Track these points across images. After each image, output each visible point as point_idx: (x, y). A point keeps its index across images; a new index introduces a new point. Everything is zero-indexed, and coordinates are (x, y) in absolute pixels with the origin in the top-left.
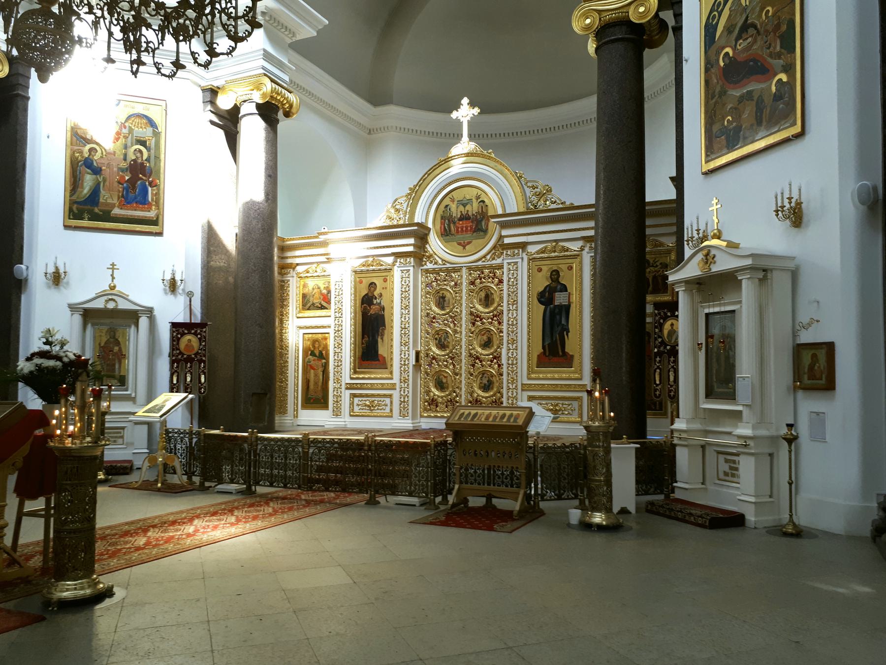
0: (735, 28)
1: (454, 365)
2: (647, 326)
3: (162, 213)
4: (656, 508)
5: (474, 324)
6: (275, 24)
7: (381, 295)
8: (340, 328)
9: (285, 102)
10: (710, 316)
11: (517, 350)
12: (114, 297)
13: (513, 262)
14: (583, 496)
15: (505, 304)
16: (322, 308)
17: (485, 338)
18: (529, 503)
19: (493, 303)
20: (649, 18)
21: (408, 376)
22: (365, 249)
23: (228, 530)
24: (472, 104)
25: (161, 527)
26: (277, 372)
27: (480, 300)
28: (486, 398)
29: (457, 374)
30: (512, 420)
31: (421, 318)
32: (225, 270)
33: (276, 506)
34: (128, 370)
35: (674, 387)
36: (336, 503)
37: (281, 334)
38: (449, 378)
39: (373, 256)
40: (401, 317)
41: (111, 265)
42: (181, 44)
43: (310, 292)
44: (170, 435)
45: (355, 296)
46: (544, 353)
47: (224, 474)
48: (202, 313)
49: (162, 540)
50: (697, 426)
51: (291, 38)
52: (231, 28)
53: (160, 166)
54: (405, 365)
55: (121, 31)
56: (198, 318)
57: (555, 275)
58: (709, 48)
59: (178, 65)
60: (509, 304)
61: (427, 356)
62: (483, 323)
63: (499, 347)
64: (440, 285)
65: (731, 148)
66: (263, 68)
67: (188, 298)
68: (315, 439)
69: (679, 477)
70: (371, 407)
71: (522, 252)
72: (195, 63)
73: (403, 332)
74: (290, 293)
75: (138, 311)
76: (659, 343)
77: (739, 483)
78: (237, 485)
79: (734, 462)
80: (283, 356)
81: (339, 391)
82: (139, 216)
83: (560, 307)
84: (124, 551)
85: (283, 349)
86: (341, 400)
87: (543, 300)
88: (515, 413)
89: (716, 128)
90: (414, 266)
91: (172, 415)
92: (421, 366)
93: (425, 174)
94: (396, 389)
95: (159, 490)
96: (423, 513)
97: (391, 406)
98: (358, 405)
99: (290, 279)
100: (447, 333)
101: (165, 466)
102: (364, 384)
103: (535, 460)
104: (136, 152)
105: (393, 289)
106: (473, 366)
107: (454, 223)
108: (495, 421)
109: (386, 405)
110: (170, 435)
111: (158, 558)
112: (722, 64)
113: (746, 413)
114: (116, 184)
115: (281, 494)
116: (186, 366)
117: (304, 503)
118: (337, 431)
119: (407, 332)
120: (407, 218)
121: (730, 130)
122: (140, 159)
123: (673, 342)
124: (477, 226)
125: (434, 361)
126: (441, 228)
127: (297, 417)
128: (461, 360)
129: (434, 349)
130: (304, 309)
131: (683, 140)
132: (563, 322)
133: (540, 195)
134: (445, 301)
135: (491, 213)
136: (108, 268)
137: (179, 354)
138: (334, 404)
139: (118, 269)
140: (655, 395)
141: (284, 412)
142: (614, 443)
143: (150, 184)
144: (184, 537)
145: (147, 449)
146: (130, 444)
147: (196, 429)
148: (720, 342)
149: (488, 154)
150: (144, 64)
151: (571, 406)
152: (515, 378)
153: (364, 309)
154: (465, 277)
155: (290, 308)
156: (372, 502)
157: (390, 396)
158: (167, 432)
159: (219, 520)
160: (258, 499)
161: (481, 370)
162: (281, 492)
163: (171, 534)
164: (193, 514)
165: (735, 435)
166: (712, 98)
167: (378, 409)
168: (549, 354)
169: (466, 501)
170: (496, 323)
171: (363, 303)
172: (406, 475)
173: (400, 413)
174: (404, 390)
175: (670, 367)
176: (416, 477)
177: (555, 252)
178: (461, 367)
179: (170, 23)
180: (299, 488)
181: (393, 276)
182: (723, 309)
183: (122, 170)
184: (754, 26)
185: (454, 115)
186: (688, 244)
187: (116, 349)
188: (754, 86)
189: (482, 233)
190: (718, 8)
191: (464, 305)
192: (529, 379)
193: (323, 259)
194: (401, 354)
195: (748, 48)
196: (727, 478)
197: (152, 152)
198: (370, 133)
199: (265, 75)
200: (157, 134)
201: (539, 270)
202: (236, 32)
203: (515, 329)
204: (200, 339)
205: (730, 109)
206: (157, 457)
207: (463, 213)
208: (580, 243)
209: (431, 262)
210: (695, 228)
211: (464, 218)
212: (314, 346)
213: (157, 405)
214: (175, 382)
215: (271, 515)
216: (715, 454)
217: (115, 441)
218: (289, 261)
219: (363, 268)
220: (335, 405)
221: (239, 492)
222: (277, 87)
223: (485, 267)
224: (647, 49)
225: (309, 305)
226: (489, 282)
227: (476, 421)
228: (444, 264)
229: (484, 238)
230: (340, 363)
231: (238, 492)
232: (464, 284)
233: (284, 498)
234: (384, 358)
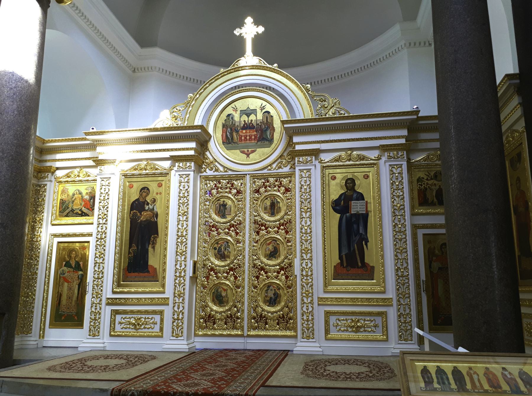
5: (258, 233)
7: (154, 201)
11: (311, 260)
17: (270, 247)
21: (184, 289)
24: (257, 23)
26: (22, 285)
27: (265, 208)
28: (272, 313)
29: (238, 287)
31: (199, 226)
37: (33, 229)
38: (229, 291)
39: (147, 159)
40: (178, 224)
45: (124, 201)
46: (341, 263)
54: (180, 277)
60: (301, 212)
70: (136, 326)
73: (179, 240)
74: (46, 199)
80: (32, 267)
81: (98, 307)
86: (99, 318)
87: (338, 208)
90: (194, 172)
94: (168, 304)
97: (161, 324)
98: (120, 323)
99: (48, 183)
100: (228, 242)
106: (258, 277)
107: (237, 132)
119: (185, 240)
125: (212, 273)
126: (222, 135)
127: (43, 337)
129: (213, 259)
130: (60, 216)
132: (361, 231)
134: (226, 209)
138: (90, 322)
141: (27, 330)
151: (374, 322)
153: (133, 216)
154: (248, 185)
155: (45, 214)
157: (161, 313)
167: (145, 328)
168: (347, 266)
173: (173, 333)
174: (179, 306)
178: (243, 279)
181: (169, 180)
189: (267, 143)
191: (248, 213)
192: (325, 292)
194: (176, 265)
198: (134, 71)
203: (309, 238)
209: (211, 169)
211: (248, 126)
212: (70, 257)
218: (48, 164)
219: (135, 172)
220: (92, 324)
225: (67, 211)
226: (275, 191)
228: (226, 172)
229: (269, 147)
232: (248, 191)
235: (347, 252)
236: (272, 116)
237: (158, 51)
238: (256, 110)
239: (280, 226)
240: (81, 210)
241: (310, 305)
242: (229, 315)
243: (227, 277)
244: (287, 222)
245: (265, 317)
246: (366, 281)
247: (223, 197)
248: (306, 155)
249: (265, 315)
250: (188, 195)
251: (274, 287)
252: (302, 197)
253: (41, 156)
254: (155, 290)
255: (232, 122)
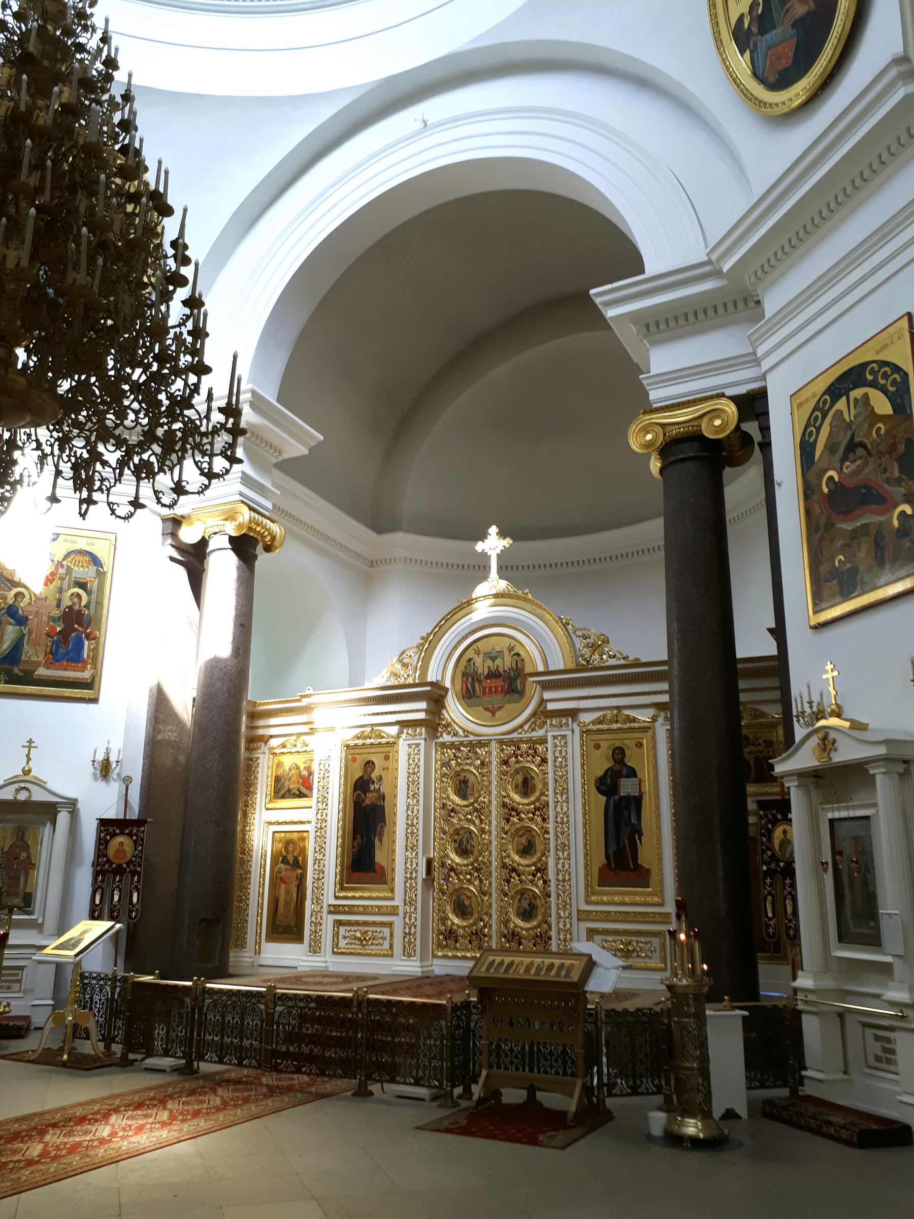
0: (838, 448)
1: (481, 881)
2: (751, 828)
3: (99, 674)
4: (778, 1111)
5: (508, 820)
6: (258, 442)
7: (380, 778)
8: (324, 824)
9: (266, 533)
10: (836, 824)
11: (569, 860)
12: (27, 785)
13: (560, 736)
14: (670, 1090)
15: (551, 792)
16: (301, 795)
17: (524, 840)
18: (590, 1100)
19: (533, 790)
20: (728, 432)
21: (416, 895)
22: (364, 716)
23: (156, 1134)
24: (502, 534)
25: (63, 1126)
27: (516, 786)
28: (527, 930)
30: (563, 973)
32: (175, 745)
33: (225, 1094)
34: (37, 884)
35: (794, 922)
36: (311, 1093)
37: (244, 832)
38: (473, 899)
40: (407, 810)
41: (27, 742)
42: (142, 483)
43: (285, 774)
44: (86, 981)
46: (608, 865)
47: (156, 1043)
48: (141, 806)
49: (65, 1148)
50: (829, 983)
51: (276, 457)
52: (205, 465)
53: (102, 613)
54: (411, 878)
55: (71, 468)
56: (134, 814)
57: (619, 754)
58: (808, 470)
59: (136, 504)
60: (556, 793)
61: (443, 866)
62: (520, 819)
63: (543, 854)
64: (461, 764)
65: (846, 594)
66: (241, 494)
67: (125, 786)
68: (283, 994)
69: (809, 1061)
70: (362, 941)
71: (573, 721)
72: (157, 503)
74: (259, 776)
75: (57, 803)
76: (769, 857)
77: (897, 1074)
78: (173, 1059)
79: (888, 1040)
80: (245, 863)
82: (69, 678)
83: (628, 798)
84: (11, 1165)
85: (245, 854)
86: (320, 930)
87: (603, 788)
88: (567, 962)
89: (824, 569)
90: (425, 739)
91: (89, 954)
92: (434, 880)
93: (442, 620)
94: (398, 915)
95: (64, 1065)
96: (437, 1113)
97: (391, 939)
98: (345, 937)
99: (261, 756)
100: (470, 832)
101: (75, 1026)
102: (354, 906)
103: (598, 1032)
104: (73, 597)
105: (397, 769)
106: (508, 881)
107: (480, 682)
108: (539, 975)
109: (385, 939)
110: (86, 981)
111: (56, 1178)
112: (826, 490)
113: (898, 966)
114: (44, 637)
115: (233, 1075)
116: (114, 880)
117: (265, 1090)
118: (315, 976)
120: (417, 675)
121: (843, 573)
122: (78, 605)
123: (787, 856)
124: (510, 685)
125: (514, 874)
126: (462, 688)
127: (259, 953)
128: (491, 873)
129: (453, 856)
131: (781, 583)
133: (594, 647)
135: (527, 671)
136: (23, 746)
137: (106, 863)
139: (37, 747)
140: (768, 934)
141: (242, 945)
142: (710, 1009)
143: (88, 637)
144: (95, 1143)
145: (52, 999)
146: (29, 991)
147: (121, 974)
148: (852, 861)
149: (523, 595)
150: (95, 503)
151: (649, 945)
152: (568, 902)
153: (356, 798)
155: (258, 796)
156: (362, 1093)
157: (390, 925)
158: (82, 976)
159: (146, 1116)
160: (201, 1082)
161: (519, 887)
162: (236, 1073)
163: (77, 1139)
164: (110, 1105)
165: (885, 1001)
166: (817, 531)
167: (372, 944)
168: (615, 869)
169: (497, 1094)
170: (539, 819)
171: (355, 789)
172: (411, 1050)
175: (786, 892)
176: (425, 1055)
177: (617, 722)
178: (490, 884)
179: (131, 458)
180: (259, 1067)
181: (397, 752)
182: (852, 813)
183: (54, 620)
184: (863, 445)
185: (480, 547)
186: (798, 721)
187: (24, 855)
188: (870, 518)
189: (516, 696)
190: (815, 423)
191: (494, 792)
192: (588, 902)
193: (305, 729)
195: (855, 473)
196: (880, 1065)
197: (94, 596)
198: (372, 565)
199: (242, 502)
200: (101, 575)
201: (597, 746)
202: (210, 468)
204: (135, 842)
205: (841, 546)
206: (66, 1014)
207: (492, 669)
208: (652, 712)
209: (449, 733)
210: (806, 699)
211: (493, 675)
212: (286, 849)
213: (71, 939)
214: (97, 902)
215: (218, 1109)
216: (860, 1027)
217: (9, 987)
218: (261, 732)
221: (176, 1070)
222: (257, 516)
223: (521, 741)
224: (727, 469)
225: (283, 792)
226: (528, 761)
227: (511, 975)
228: (467, 736)
229: (520, 702)
230: (321, 875)
231: (174, 1071)
233: (238, 1082)
234: (383, 868)
235: (615, 848)
236: (523, 660)
237: (399, 537)
238: (503, 652)
239: (535, 811)
240: (298, 790)
241: (568, 920)
242: (474, 931)
243: (533, 880)
244: (544, 806)
245: (518, 935)
246: (640, 889)
247: (462, 770)
248: (560, 716)
249: (518, 932)
250: (418, 772)
251: (528, 895)
252: (557, 773)
253: (252, 722)
254: (381, 895)
255: (474, 670)
